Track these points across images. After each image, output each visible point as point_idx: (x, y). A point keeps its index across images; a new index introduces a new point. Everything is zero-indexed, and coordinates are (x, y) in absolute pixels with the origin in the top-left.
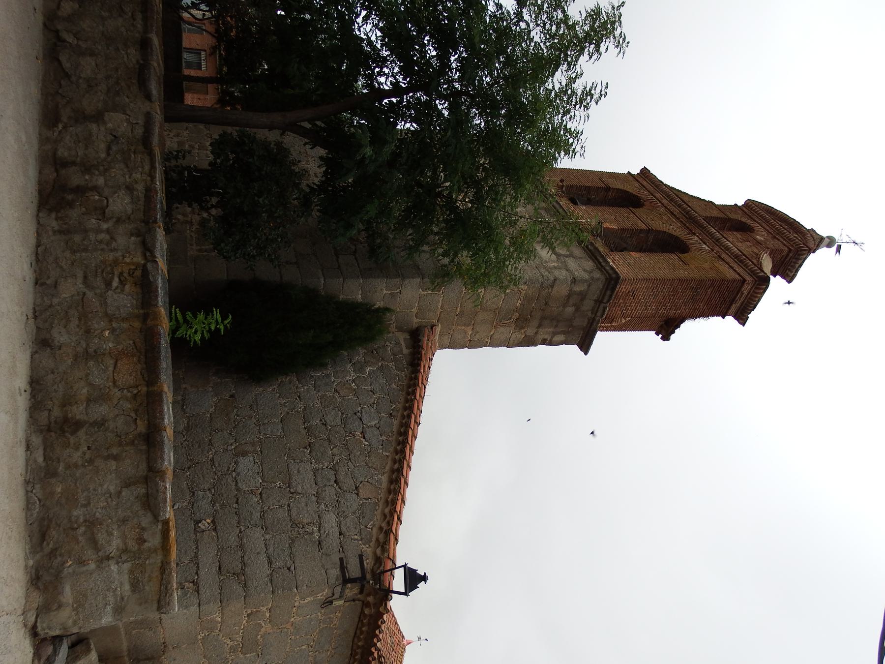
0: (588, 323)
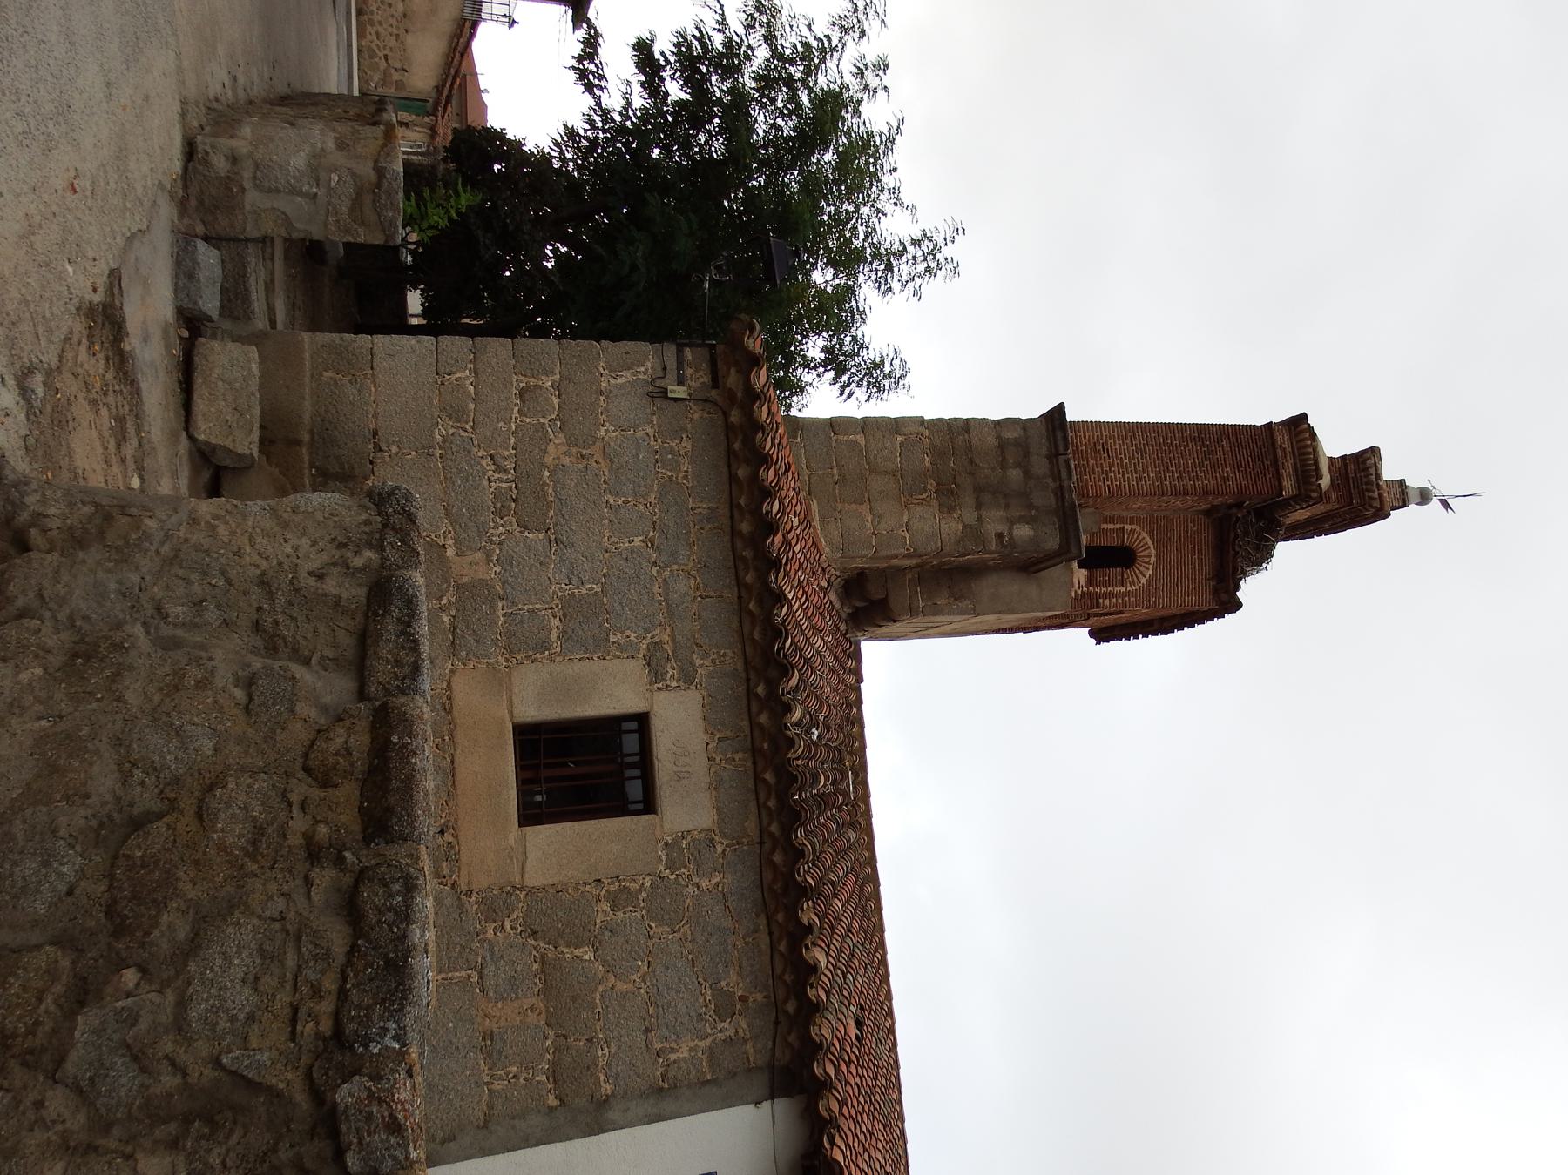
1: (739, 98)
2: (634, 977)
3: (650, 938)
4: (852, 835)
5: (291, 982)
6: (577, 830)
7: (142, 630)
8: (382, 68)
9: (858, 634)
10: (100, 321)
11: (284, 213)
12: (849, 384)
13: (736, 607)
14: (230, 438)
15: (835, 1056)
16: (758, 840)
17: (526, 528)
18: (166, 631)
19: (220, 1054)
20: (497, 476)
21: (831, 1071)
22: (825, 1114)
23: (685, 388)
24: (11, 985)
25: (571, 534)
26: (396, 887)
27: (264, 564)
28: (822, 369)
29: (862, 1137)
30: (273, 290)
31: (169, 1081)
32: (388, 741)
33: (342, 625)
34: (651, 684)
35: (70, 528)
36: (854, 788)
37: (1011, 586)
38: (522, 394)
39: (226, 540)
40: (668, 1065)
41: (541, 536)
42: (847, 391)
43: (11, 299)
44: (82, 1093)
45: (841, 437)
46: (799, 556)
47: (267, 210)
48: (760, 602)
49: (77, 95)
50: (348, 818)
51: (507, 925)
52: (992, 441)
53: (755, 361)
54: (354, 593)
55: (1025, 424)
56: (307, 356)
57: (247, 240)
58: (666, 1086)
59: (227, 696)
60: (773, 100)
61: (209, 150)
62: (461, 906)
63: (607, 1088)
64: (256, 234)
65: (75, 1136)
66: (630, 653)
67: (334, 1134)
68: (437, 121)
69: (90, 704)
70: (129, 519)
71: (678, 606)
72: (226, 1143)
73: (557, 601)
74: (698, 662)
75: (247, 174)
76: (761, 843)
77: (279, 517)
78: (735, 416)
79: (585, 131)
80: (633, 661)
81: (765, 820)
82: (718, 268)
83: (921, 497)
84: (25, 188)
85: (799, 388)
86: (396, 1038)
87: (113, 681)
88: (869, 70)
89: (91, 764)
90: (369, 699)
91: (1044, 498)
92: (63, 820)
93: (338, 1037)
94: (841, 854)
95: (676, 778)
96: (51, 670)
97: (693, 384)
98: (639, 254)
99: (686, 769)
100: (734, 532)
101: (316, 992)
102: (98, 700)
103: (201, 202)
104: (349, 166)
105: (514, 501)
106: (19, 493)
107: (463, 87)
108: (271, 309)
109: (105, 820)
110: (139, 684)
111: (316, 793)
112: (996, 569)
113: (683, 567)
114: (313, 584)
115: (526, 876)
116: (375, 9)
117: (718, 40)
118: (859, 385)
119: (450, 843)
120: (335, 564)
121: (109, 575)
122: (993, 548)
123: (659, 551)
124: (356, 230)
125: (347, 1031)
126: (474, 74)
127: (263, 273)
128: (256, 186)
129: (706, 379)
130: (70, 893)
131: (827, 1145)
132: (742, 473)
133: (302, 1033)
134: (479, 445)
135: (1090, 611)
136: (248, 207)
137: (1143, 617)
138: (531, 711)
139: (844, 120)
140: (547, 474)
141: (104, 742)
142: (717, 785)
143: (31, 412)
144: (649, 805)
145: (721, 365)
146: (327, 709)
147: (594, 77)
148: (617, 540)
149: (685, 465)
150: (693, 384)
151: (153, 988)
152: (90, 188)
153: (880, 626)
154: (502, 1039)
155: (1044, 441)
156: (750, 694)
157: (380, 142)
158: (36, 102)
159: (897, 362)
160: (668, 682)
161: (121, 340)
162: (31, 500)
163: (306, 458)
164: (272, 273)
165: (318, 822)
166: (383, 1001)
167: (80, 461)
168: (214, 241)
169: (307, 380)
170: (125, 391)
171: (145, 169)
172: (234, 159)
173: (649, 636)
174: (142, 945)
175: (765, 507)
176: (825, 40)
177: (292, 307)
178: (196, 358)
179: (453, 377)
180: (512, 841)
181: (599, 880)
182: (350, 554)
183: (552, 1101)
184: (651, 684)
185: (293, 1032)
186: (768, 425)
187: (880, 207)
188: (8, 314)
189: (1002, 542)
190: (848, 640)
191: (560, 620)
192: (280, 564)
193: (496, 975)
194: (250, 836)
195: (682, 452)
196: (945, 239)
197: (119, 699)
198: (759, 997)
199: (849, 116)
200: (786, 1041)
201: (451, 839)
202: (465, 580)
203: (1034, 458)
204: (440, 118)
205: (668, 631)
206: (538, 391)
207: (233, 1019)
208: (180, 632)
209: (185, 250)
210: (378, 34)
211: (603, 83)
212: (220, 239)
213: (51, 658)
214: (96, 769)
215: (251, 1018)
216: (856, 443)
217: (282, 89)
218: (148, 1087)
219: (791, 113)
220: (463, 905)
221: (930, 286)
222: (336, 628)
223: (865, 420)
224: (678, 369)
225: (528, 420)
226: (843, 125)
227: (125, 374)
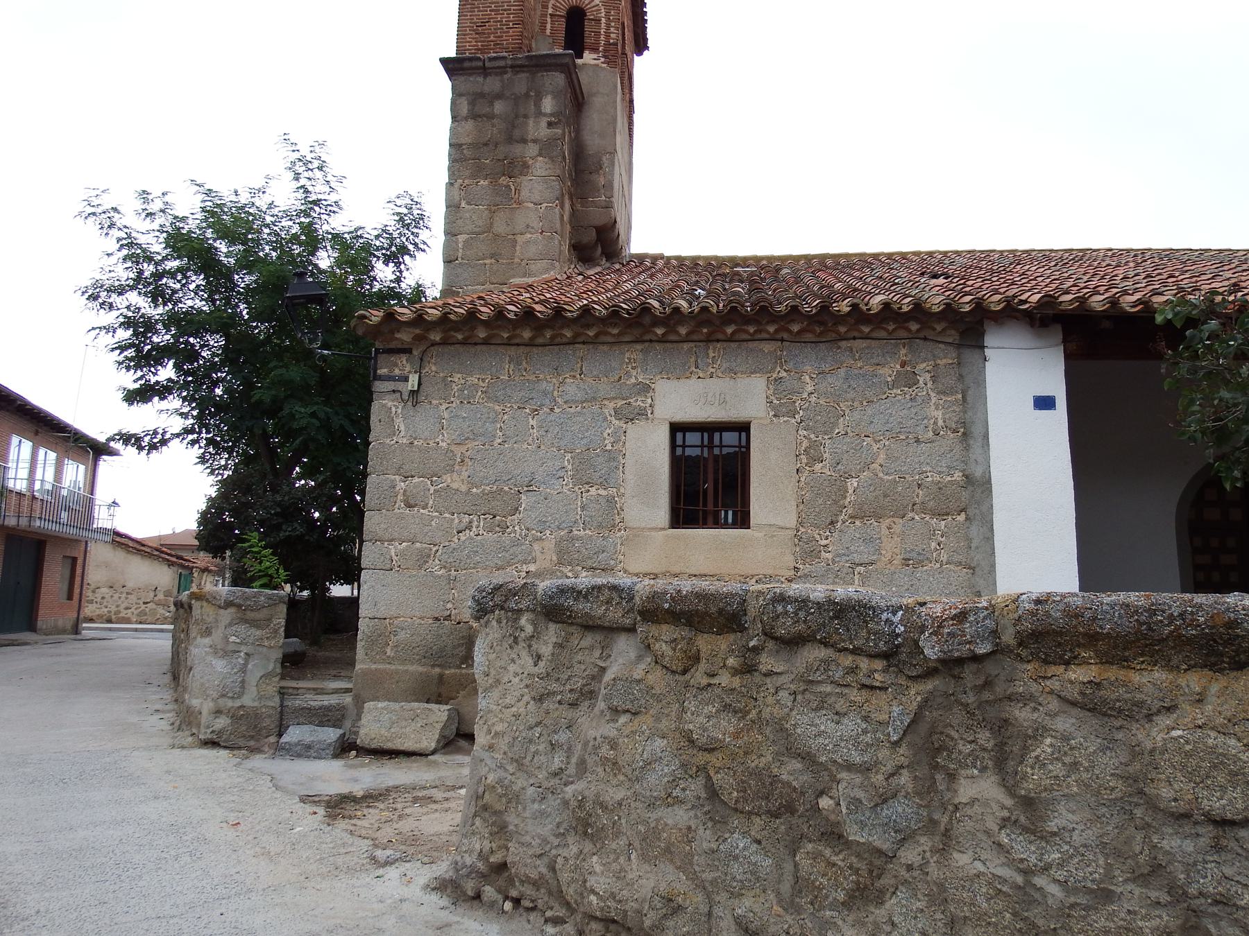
0: (523, 72)
1: (173, 320)
2: (875, 448)
3: (846, 434)
4: (785, 271)
5: (843, 689)
6: (757, 485)
7: (570, 787)
8: (154, 606)
9: (623, 255)
10: (339, 811)
11: (261, 678)
12: (416, 245)
14: (434, 724)
15: (957, 295)
16: (780, 342)
17: (517, 509)
18: (572, 770)
19: (889, 742)
20: (474, 529)
21: (968, 298)
22: (1002, 306)
23: (411, 376)
24: (821, 883)
25: (523, 474)
26: (780, 608)
27: (526, 698)
28: (402, 267)
29: (1024, 281)
30: (322, 689)
31: (905, 778)
32: (667, 611)
33: (576, 643)
34: (648, 419)
35: (491, 834)
36: (748, 267)
37: (593, 120)
38: (409, 506)
39: (506, 725)
40: (946, 427)
41: (523, 497)
42: (421, 246)
43: (318, 869)
44: (906, 838)
45: (460, 255)
46: (554, 295)
48: (588, 326)
49: (164, 819)
50: (723, 643)
51: (824, 542)
52: (469, 125)
53: (390, 316)
54: (552, 633)
55: (457, 94)
56: (374, 667)
57: (282, 706)
58: (962, 430)
59: (624, 728)
60: (174, 292)
61: (211, 729)
62: (806, 576)
63: (958, 476)
64: (277, 699)
65: (936, 844)
66: (619, 437)
67: (960, 661)
68: (196, 567)
69: (621, 824)
70: (486, 793)
71: (587, 393)
72: (956, 740)
73: (576, 488)
74: (633, 380)
75: (230, 703)
76: (782, 340)
77: (491, 686)
78: (436, 336)
79: (200, 447)
80: (628, 432)
81: (764, 335)
82: (311, 341)
83: (513, 190)
84: (234, 857)
85: (419, 291)
86: (894, 613)
87: (606, 808)
88: (148, 208)
89: (666, 825)
90: (635, 624)
91: (521, 83)
92: (705, 845)
93: (885, 656)
94: (798, 280)
95: (724, 405)
96: (595, 850)
97: (408, 369)
98: (303, 410)
99: (718, 396)
100: (531, 344)
101: (853, 670)
102: (619, 819)
103: (252, 737)
105: (495, 517)
106: (463, 868)
107: (171, 546)
108: (336, 691)
109: (708, 816)
110: (610, 790)
111: (703, 666)
112: (578, 131)
114: (544, 662)
115: (788, 526)
116: (106, 610)
117: (124, 335)
118: (417, 235)
119: (757, 582)
120: (530, 646)
121: (528, 808)
122: (559, 131)
123: (542, 406)
125: (884, 649)
126: (160, 537)
127: (307, 696)
128: (239, 697)
129: (404, 358)
130: (759, 842)
131: (1027, 306)
132: (482, 334)
133: (881, 682)
135: (620, 52)
136: (256, 704)
137: (629, 7)
138: (661, 512)
139: (190, 232)
140: (474, 490)
141: (651, 815)
142: (732, 373)
143: (404, 859)
144: (743, 428)
145: (393, 345)
146: (640, 656)
147: (155, 438)
149: (473, 380)
151: (835, 787)
152: (236, 814)
153: (619, 235)
154: (910, 552)
155: (471, 79)
156: (662, 340)
157: (205, 604)
158: (167, 847)
159: (399, 202)
160: (648, 405)
161: (355, 797)
162: (468, 860)
163: (453, 671)
164: (309, 689)
165: (724, 665)
166: (866, 622)
167: (446, 828)
168: (282, 730)
169: (393, 667)
170: (394, 796)
171: (224, 775)
172: (218, 712)
173: (609, 418)
174: (803, 794)
175: (511, 316)
176: (121, 243)
177: (336, 677)
178: (373, 746)
179: (395, 558)
180: (760, 535)
181: (798, 470)
182: (523, 635)
183: (962, 517)
184: (648, 419)
185: (880, 688)
186: (443, 309)
187: (266, 206)
188: (329, 872)
189: (556, 123)
190: (628, 263)
191: (591, 487)
192: (527, 686)
193: (861, 553)
194: (730, 715)
195: (463, 381)
196: (294, 151)
197: (620, 804)
198: (903, 351)
199: (186, 227)
200: (940, 332)
201: (754, 580)
202: (554, 558)
203: (486, 89)
204: (195, 565)
205: (606, 402)
207: (865, 732)
208: (574, 760)
209: (288, 751)
210: (127, 608)
211: (160, 431)
212: (281, 725)
213: (586, 851)
214: (670, 822)
215: (866, 719)
216: (465, 242)
217: (168, 678)
218: (908, 793)
219: (185, 277)
220: (805, 575)
221: (334, 168)
222: (579, 647)
223: (447, 233)
224: (395, 380)
225: (431, 502)
226: (195, 233)
227: (380, 795)
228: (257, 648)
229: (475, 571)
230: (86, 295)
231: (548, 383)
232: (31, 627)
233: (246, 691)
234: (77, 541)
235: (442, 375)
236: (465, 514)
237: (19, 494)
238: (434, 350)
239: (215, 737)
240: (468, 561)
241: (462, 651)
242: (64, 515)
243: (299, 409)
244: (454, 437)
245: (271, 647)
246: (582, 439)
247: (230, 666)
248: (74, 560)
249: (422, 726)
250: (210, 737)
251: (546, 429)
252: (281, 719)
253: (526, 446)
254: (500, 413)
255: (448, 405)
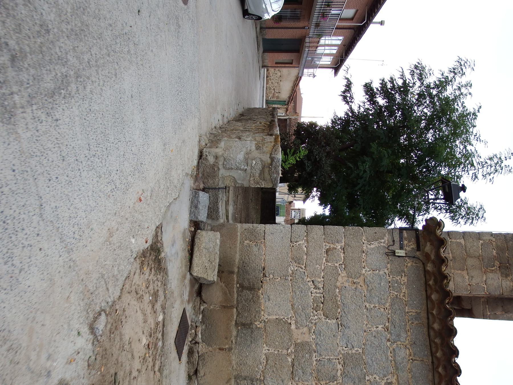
8: (273, 93)
11: (233, 177)
13: (431, 367)
14: (206, 274)
17: (327, 317)
20: (315, 291)
25: (348, 321)
30: (228, 204)
38: (327, 251)
41: (334, 321)
45: (453, 240)
47: (227, 176)
56: (239, 234)
57: (219, 188)
61: (208, 154)
64: (222, 186)
71: (400, 364)
73: (341, 356)
75: (221, 163)
83: (492, 269)
97: (408, 249)
98: (367, 167)
103: (203, 175)
104: (260, 157)
105: (322, 303)
108: (227, 211)
113: (403, 343)
124: (261, 182)
128: (224, 167)
129: (414, 246)
134: (308, 276)
136: (220, 176)
140: (337, 290)
145: (422, 240)
148: (370, 326)
150: (408, 249)
157: (273, 144)
163: (236, 279)
164: (228, 198)
169: (238, 245)
173: (385, 378)
178: (196, 240)
179: (298, 243)
191: (342, 366)
195: (402, 283)
202: (299, 341)
205: (395, 377)
206: (334, 250)
210: (272, 83)
223: (464, 233)
224: (400, 241)
225: (330, 264)
228: (249, 175)
229: (291, 291)
230: (417, 64)
231: (405, 338)
232: (265, 51)
233: (227, 171)
234: (299, 64)
235: (406, 269)
236: (324, 285)
237: (319, 42)
238: (420, 265)
239: (204, 157)
240: (296, 287)
241: (246, 284)
242: (310, 59)
243: (367, 165)
244: (368, 277)
245: (249, 181)
246: (372, 360)
247: (240, 161)
248: (292, 63)
249: (205, 266)
250: (204, 154)
251: (376, 336)
252: (212, 189)
253: (365, 323)
254: (385, 306)
255: (387, 273)
